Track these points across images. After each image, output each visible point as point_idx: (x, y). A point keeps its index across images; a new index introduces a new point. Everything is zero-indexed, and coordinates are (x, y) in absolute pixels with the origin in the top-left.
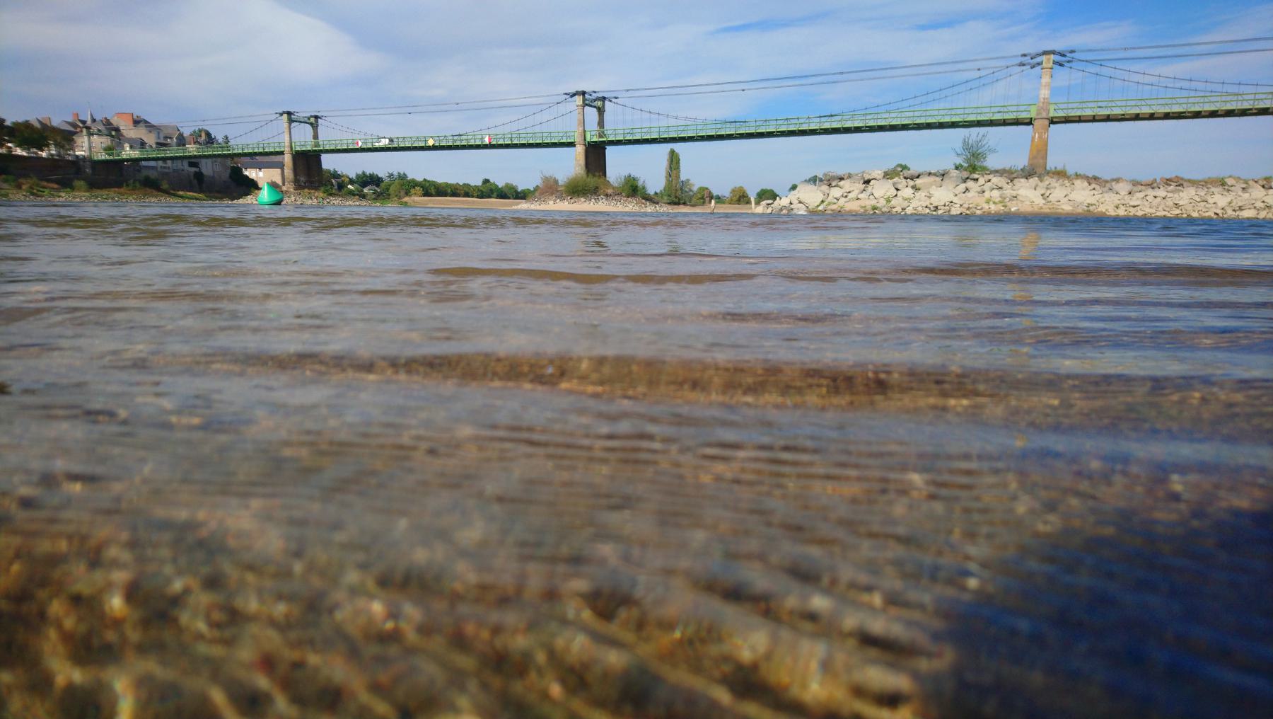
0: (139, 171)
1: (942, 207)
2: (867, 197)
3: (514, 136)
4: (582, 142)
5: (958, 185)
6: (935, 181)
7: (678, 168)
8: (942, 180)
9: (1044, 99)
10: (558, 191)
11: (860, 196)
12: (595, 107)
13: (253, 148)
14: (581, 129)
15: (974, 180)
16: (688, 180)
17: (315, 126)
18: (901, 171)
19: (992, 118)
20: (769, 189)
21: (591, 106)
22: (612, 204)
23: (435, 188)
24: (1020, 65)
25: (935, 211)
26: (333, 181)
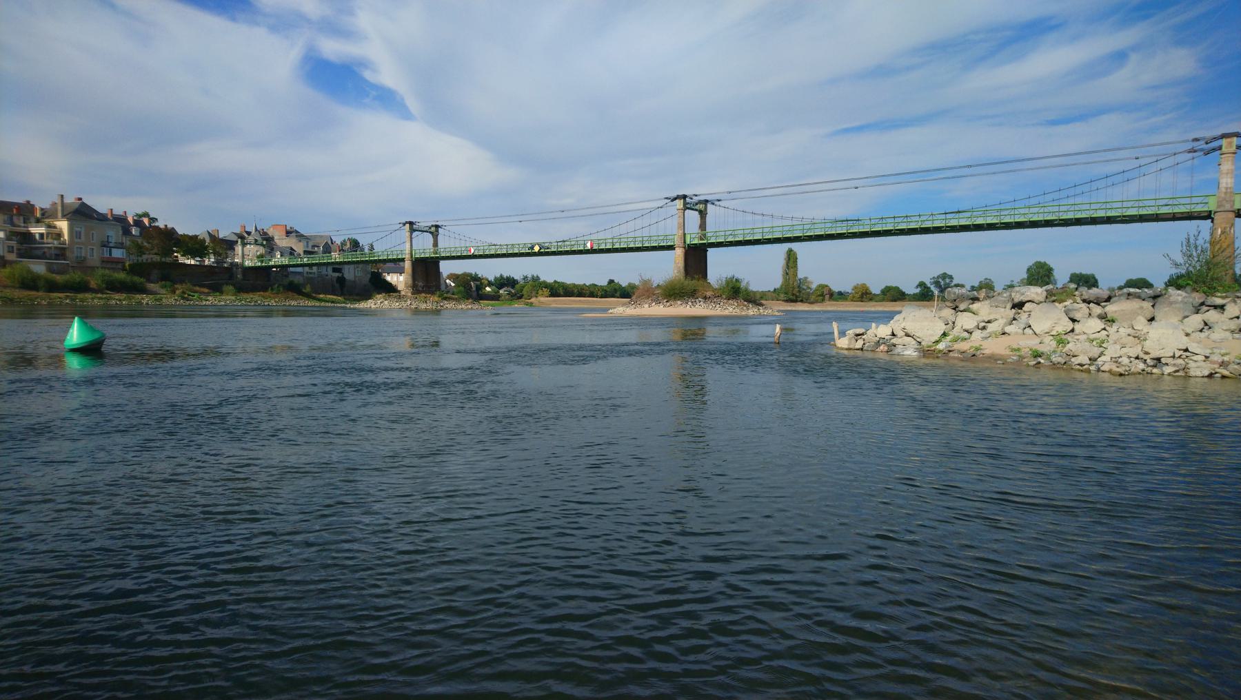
0: (287, 276)
1: (1170, 361)
2: (1020, 331)
3: (615, 241)
4: (682, 245)
5: (1187, 317)
6: (1142, 308)
7: (795, 266)
8: (1153, 306)
9: (1227, 188)
10: (654, 295)
11: (1008, 329)
12: (696, 210)
13: (398, 255)
14: (681, 232)
15: (1215, 307)
16: (806, 278)
17: (435, 236)
18: (1077, 289)
19: (1158, 212)
20: (894, 286)
21: (693, 209)
22: (711, 307)
23: (563, 289)
24: (1189, 152)
25: (1155, 366)
26: (472, 283)
